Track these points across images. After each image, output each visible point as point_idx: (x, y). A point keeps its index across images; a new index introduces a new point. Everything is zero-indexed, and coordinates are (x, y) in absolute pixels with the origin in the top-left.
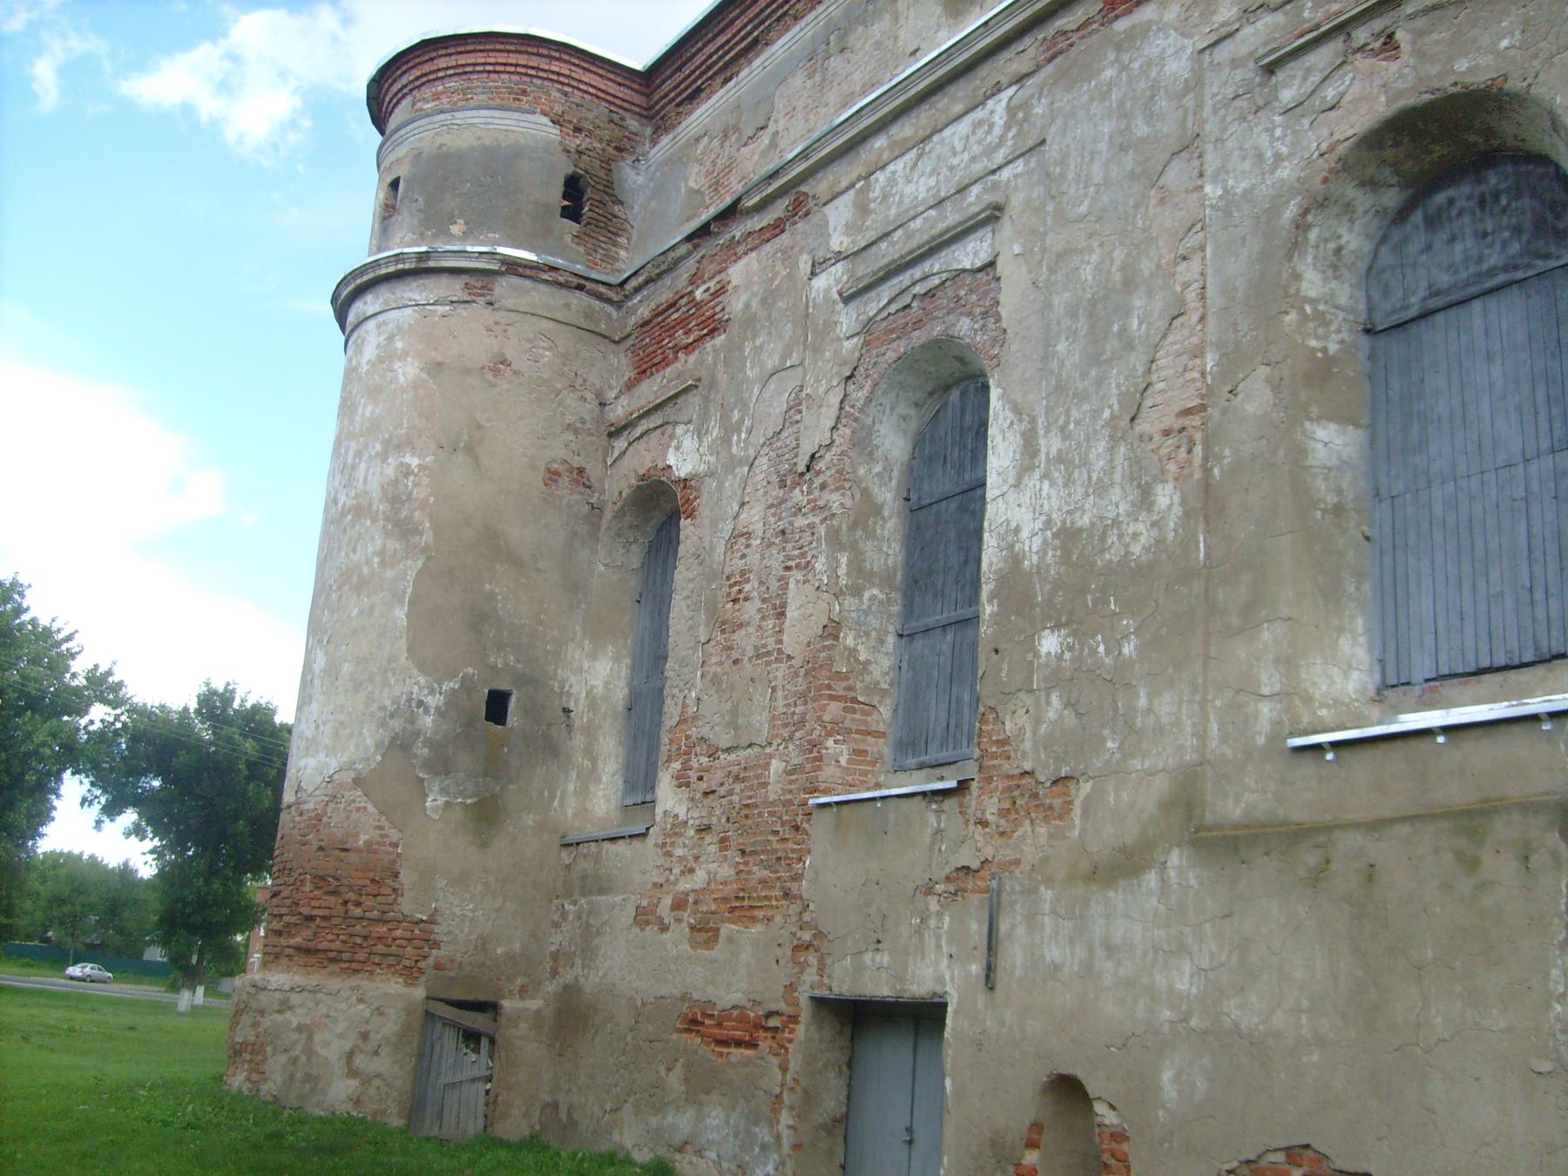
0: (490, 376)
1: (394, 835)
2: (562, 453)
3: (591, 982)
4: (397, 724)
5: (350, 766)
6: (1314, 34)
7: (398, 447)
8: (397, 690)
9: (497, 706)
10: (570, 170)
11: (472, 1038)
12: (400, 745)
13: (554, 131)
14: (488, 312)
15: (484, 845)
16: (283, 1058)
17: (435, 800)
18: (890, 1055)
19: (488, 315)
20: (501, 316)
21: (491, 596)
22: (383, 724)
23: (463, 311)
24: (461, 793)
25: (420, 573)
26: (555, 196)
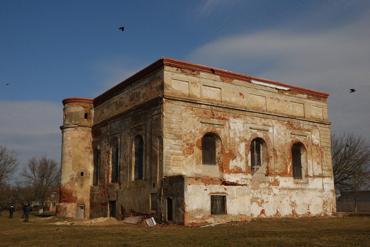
0: (78, 138)
1: (72, 188)
2: (87, 145)
3: (222, 133)
4: (72, 177)
5: (67, 182)
6: (119, 156)
7: (69, 147)
8: (71, 173)
9: (82, 174)
10: (85, 113)
11: (82, 208)
12: (72, 179)
13: (83, 108)
14: (77, 131)
15: (82, 189)
16: (62, 212)
17: (76, 184)
18: (280, 202)
19: (77, 132)
20: (79, 132)
21: (80, 163)
22: (70, 177)
23: (74, 131)
24: (79, 183)
25: (73, 161)
26: (84, 116)
